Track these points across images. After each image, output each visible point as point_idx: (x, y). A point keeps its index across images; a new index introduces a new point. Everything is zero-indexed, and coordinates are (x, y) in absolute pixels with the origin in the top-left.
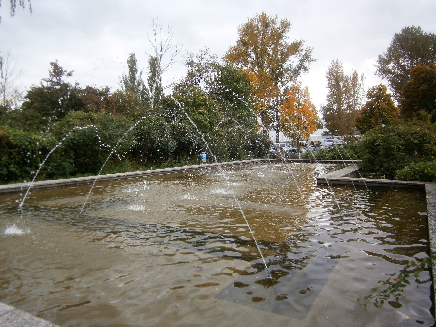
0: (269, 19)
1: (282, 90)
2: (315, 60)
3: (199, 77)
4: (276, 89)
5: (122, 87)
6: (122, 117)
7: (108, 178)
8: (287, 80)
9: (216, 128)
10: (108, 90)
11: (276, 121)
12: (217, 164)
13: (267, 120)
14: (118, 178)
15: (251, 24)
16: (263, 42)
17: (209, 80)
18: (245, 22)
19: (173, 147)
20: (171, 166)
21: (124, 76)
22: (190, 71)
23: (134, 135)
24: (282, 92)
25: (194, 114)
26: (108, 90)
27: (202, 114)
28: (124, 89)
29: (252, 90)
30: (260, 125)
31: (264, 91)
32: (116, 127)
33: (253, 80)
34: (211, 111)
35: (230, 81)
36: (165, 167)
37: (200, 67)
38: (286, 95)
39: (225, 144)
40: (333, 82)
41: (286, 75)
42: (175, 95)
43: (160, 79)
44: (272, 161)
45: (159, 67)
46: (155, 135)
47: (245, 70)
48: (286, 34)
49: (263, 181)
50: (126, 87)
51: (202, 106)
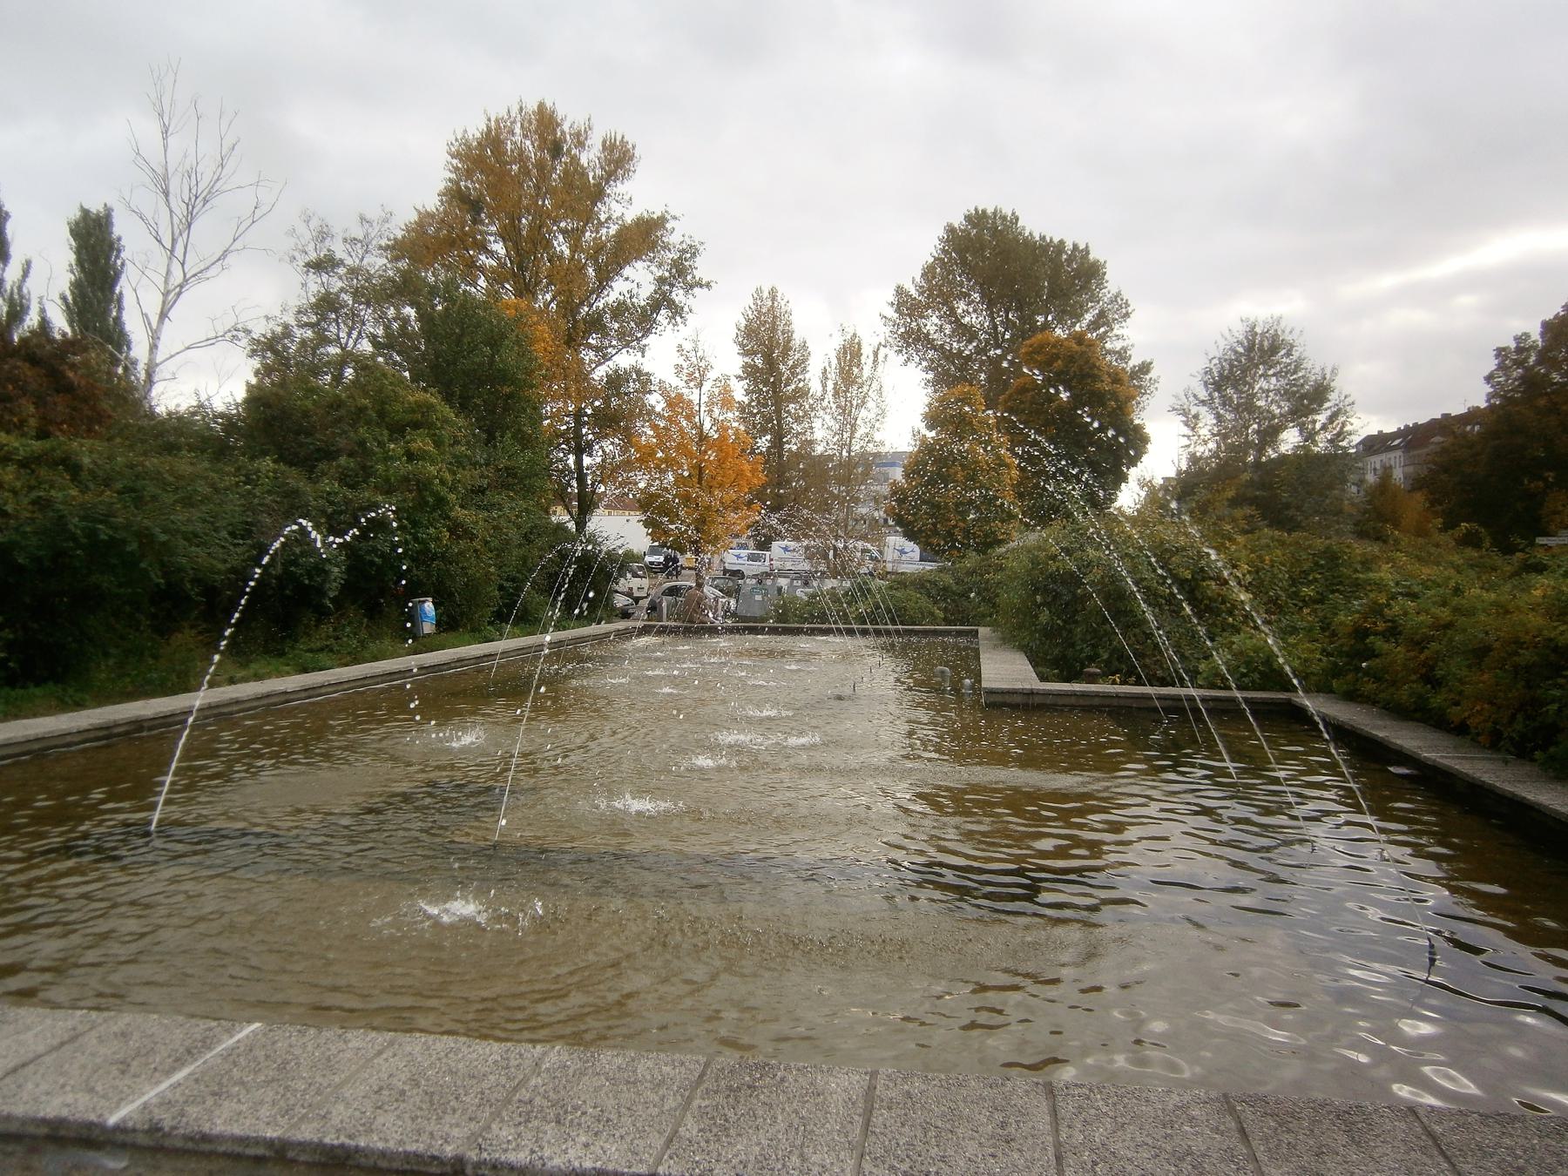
0: (566, 127)
1: (600, 373)
2: (708, 285)
15: (498, 135)
16: (530, 204)
18: (475, 128)
40: (759, 362)
48: (618, 188)
51: (416, 426)
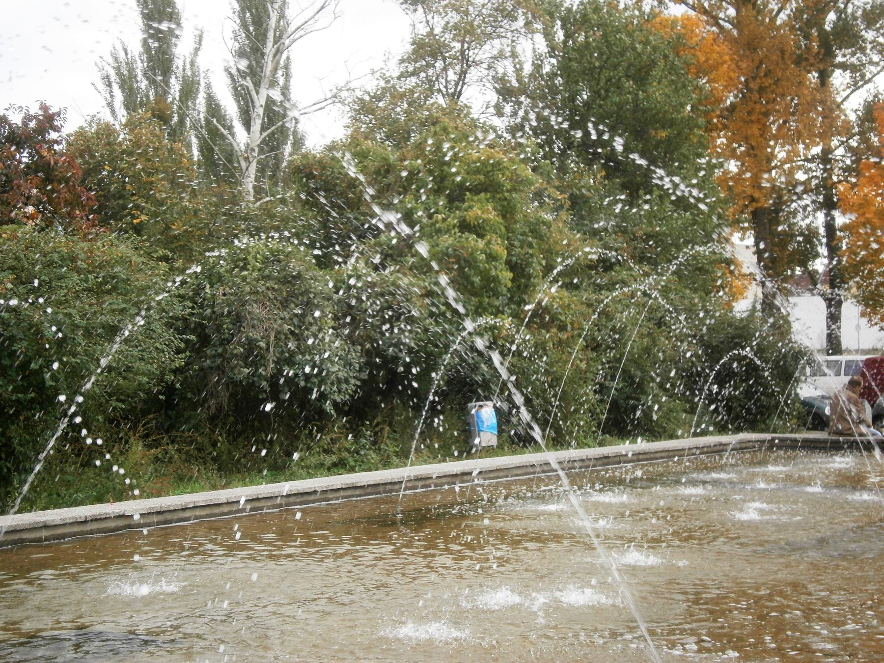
1: (853, 105)
3: (463, 56)
4: (822, 102)
5: (110, 105)
6: (113, 247)
7: (46, 527)
8: (876, 58)
9: (548, 293)
10: (48, 120)
11: (823, 250)
12: (552, 457)
13: (783, 256)
14: (94, 526)
17: (510, 70)
19: (347, 381)
20: (340, 466)
21: (122, 55)
22: (423, 30)
23: (169, 325)
24: (853, 117)
25: (439, 231)
26: (48, 120)
27: (478, 230)
28: (122, 114)
29: (706, 113)
30: (745, 270)
31: (767, 114)
32: (89, 290)
33: (716, 67)
34: (519, 216)
35: (605, 74)
36: (311, 471)
37: (467, 13)
38: (871, 129)
39: (583, 365)
41: (869, 35)
42: (354, 145)
43: (287, 67)
44: (812, 446)
45: (282, 16)
46: (264, 322)
47: (674, 22)
49: (757, 542)
50: (130, 104)
